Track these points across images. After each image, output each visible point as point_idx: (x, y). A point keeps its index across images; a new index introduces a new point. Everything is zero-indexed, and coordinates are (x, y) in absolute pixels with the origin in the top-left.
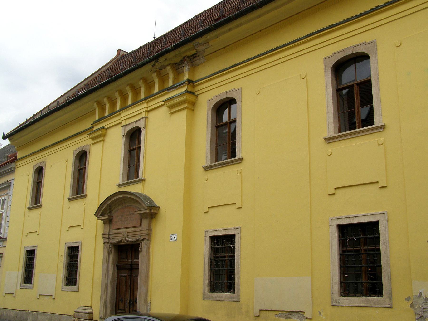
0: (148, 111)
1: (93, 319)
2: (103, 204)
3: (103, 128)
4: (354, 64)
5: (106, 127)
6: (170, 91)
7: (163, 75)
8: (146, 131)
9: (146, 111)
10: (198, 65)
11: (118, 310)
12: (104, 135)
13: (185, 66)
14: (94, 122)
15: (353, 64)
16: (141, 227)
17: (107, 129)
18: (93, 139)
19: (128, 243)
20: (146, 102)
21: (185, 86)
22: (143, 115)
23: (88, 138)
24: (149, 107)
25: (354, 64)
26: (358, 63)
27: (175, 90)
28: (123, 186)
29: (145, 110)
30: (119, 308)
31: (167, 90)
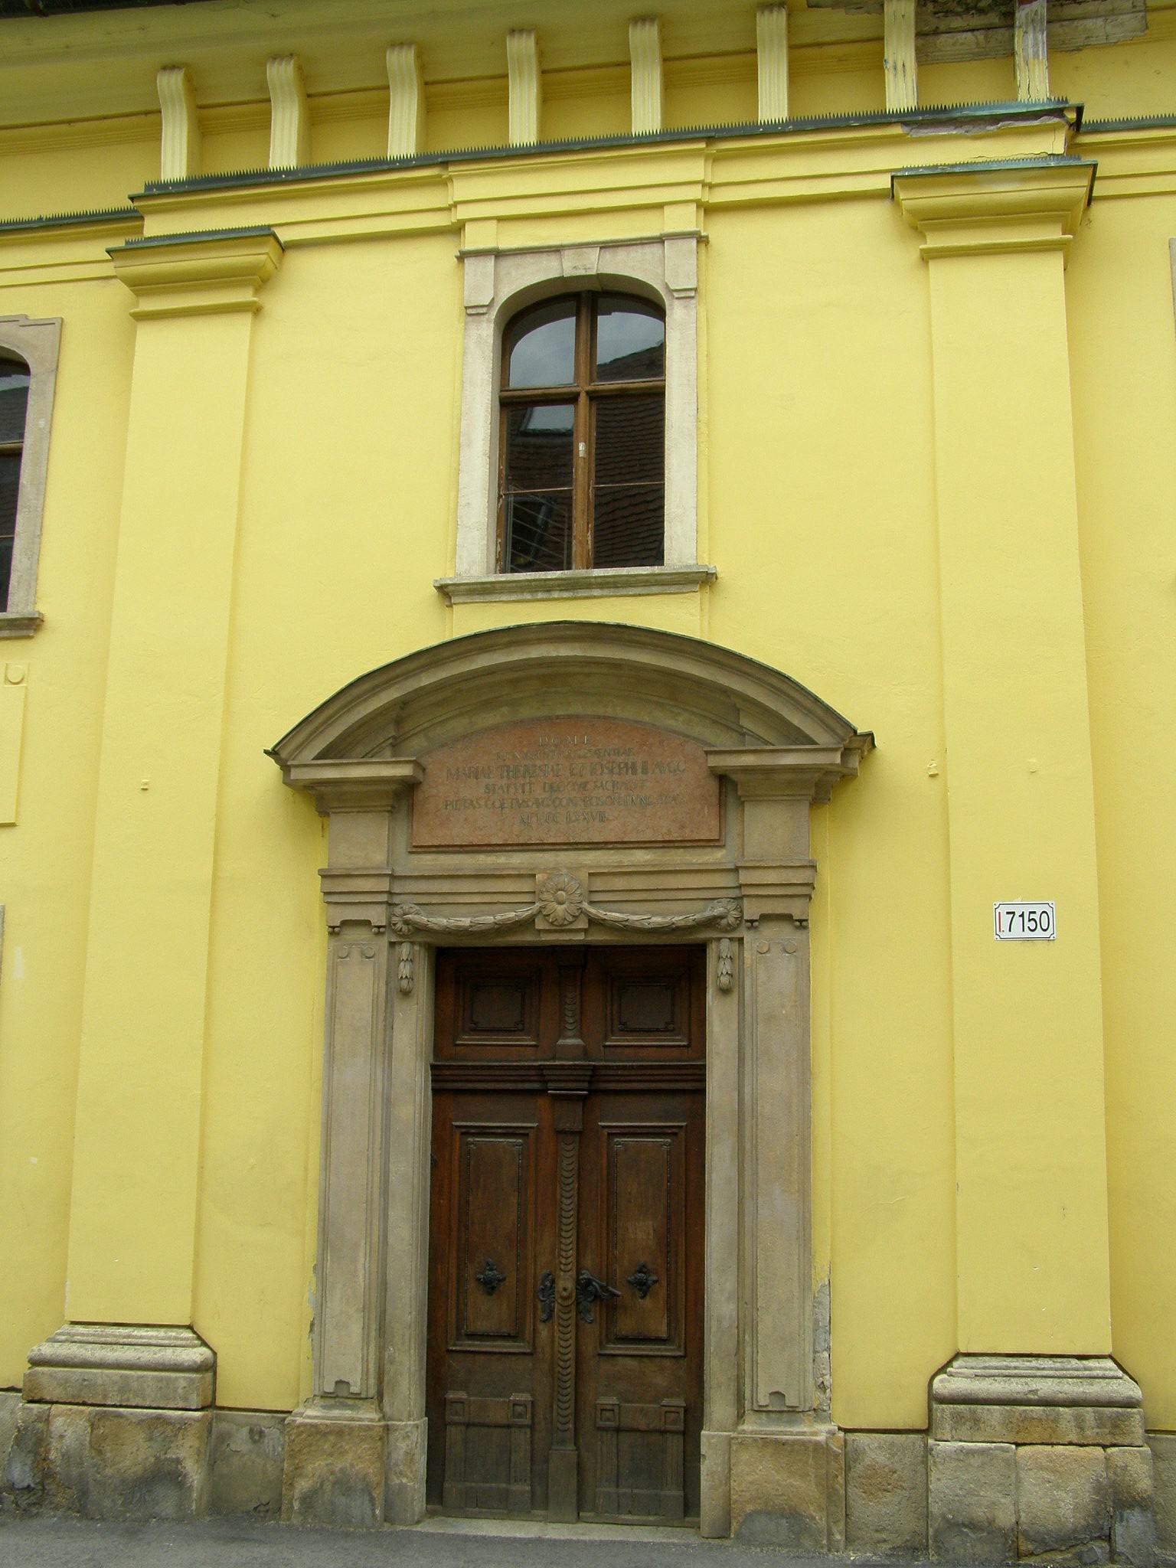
0: (709, 210)
1: (214, 1398)
2: (366, 686)
3: (265, 233)
4: (574, 318)
5: (285, 235)
6: (924, 133)
7: (809, 40)
8: (703, 319)
9: (699, 204)
10: (1079, 49)
11: (459, 1337)
12: (261, 280)
13: (1027, 27)
14: (148, 187)
15: (573, 316)
16: (723, 846)
17: (284, 248)
18: (141, 286)
19: (598, 937)
20: (707, 157)
21: (1053, 129)
22: (685, 219)
23: (108, 269)
24: (723, 189)
25: (574, 318)
26: (603, 314)
27: (967, 138)
28: (504, 598)
29: (695, 193)
30: (459, 1329)
31: (905, 124)
